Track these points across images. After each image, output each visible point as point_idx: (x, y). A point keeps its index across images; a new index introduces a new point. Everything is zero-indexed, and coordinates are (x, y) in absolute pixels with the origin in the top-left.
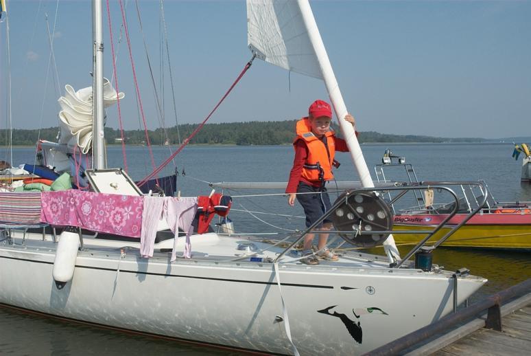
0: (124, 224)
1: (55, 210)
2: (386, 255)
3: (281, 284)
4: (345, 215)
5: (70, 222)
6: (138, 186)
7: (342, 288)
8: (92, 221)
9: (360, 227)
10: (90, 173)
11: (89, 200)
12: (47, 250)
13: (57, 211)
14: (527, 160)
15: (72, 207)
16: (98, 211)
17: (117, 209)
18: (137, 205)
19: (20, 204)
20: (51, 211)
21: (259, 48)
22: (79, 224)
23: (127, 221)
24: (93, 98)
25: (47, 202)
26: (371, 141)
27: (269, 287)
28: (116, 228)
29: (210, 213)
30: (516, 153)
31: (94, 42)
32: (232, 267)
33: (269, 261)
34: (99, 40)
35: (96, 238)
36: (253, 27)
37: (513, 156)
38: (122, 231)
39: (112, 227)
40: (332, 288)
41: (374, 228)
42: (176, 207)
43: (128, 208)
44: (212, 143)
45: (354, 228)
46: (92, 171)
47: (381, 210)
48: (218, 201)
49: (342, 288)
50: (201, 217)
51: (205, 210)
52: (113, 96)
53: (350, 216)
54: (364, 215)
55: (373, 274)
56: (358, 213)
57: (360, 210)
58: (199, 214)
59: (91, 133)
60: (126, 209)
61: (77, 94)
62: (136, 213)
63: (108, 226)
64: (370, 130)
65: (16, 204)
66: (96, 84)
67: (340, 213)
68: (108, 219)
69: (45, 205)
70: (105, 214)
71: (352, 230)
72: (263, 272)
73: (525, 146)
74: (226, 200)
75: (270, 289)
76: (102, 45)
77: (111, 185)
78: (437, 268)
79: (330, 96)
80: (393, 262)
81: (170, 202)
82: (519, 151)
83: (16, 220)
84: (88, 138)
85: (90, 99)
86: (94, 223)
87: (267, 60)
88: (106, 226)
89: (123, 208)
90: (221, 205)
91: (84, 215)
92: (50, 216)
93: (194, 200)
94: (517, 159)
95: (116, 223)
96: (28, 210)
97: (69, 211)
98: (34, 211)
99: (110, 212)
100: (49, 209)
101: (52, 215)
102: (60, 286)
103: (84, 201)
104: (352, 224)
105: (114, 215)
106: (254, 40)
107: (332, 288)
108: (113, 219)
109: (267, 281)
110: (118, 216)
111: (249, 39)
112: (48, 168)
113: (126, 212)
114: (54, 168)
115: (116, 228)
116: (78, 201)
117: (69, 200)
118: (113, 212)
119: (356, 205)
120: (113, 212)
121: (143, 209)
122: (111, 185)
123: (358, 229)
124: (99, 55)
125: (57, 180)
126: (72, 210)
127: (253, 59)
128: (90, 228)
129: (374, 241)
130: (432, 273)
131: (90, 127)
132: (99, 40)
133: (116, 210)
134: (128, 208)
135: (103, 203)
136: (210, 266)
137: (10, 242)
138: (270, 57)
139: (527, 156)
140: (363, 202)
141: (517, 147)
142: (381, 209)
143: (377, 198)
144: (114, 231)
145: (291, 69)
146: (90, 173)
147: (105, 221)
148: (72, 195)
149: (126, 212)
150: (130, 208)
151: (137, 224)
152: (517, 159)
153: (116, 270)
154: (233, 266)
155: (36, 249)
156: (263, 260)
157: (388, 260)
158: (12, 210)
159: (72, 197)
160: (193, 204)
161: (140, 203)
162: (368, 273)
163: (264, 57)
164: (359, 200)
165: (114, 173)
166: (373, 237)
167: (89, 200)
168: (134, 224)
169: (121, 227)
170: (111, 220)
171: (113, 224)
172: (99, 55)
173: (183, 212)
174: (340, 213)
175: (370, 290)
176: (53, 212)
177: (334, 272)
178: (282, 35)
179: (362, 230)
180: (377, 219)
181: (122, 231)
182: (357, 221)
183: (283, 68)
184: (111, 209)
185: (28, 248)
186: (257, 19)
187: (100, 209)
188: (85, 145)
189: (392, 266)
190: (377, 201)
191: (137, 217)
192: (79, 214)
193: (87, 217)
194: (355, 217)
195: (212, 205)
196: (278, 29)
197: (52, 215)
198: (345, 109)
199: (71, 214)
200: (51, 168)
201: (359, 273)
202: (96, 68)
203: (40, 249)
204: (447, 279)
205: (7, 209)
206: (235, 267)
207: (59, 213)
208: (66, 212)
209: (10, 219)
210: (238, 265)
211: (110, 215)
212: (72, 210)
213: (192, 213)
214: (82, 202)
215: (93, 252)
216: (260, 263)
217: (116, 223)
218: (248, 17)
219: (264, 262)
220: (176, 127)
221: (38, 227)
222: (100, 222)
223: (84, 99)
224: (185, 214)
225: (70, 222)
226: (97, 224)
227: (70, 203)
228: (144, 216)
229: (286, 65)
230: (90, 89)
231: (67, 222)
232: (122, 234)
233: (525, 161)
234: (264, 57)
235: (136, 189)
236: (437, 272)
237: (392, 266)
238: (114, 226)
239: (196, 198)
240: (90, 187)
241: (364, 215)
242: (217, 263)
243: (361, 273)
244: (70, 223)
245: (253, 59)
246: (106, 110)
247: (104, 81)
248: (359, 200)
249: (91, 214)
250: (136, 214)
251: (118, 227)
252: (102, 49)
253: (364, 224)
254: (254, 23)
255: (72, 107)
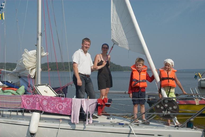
0: (63, 109)
1: (28, 103)
2: (173, 122)
3: (136, 134)
4: (160, 107)
5: (36, 108)
6: (55, 91)
7: (158, 135)
8: (48, 108)
9: (166, 112)
10: (36, 86)
11: (46, 99)
12: (24, 120)
13: (29, 103)
14: (200, 79)
15: (37, 102)
16: (51, 104)
17: (60, 103)
18: (69, 102)
19: (15, 100)
20: (26, 104)
21: (116, 40)
22: (41, 109)
23: (32, 103)
24: (37, 55)
25: (24, 100)
26: (127, 70)
27: (130, 135)
28: (60, 111)
29: (103, 106)
30: (196, 77)
31: (38, 32)
32: (111, 127)
33: (127, 125)
34: (40, 31)
35: (43, 114)
36: (113, 32)
37: (195, 78)
38: (62, 112)
39: (58, 111)
40: (154, 135)
41: (171, 112)
42: (87, 103)
43: (65, 103)
44: (61, 71)
45: (163, 112)
46: (36, 85)
47: (175, 105)
48: (107, 101)
49: (158, 135)
50: (99, 107)
51: (101, 104)
52: (44, 54)
53: (162, 108)
54: (168, 107)
55: (148, 129)
56: (165, 106)
57: (166, 105)
58: (97, 106)
59: (35, 69)
60: (64, 103)
61: (29, 52)
62: (34, 100)
63: (55, 110)
64: (127, 66)
65: (8, 100)
66: (38, 49)
67: (158, 107)
68: (56, 107)
69: (24, 101)
70: (54, 105)
71: (163, 113)
72: (126, 129)
73: (199, 74)
74: (110, 101)
75: (130, 136)
76: (41, 33)
77: (45, 91)
78: (195, 127)
79: (148, 61)
80: (176, 125)
81: (84, 101)
82: (197, 75)
83: (8, 107)
84: (34, 71)
85: (35, 55)
86: (49, 109)
87: (119, 45)
88: (55, 110)
89: (30, 98)
90: (108, 103)
91: (43, 106)
92: (26, 105)
93: (95, 100)
94: (196, 79)
95: (60, 109)
96: (15, 103)
97: (35, 104)
98: (18, 103)
99: (56, 104)
100: (25, 103)
101: (27, 105)
102: (32, 135)
103: (43, 100)
104: (163, 111)
105: (59, 106)
106: (114, 37)
107: (154, 135)
108: (58, 107)
109: (128, 133)
110: (61, 106)
111: (112, 37)
112: (9, 82)
113: (64, 104)
114: (12, 82)
115: (60, 111)
116: (40, 101)
117: (36, 99)
118: (58, 105)
119: (165, 103)
120: (58, 105)
121: (72, 103)
122: (45, 91)
123: (165, 113)
124: (40, 37)
125: (19, 89)
126: (37, 103)
127: (114, 45)
128: (47, 111)
129: (171, 117)
130: (194, 129)
131: (35, 67)
132: (40, 31)
133: (27, 99)
134: (65, 103)
135: (53, 101)
136: (101, 126)
137: (3, 116)
138: (120, 44)
139: (200, 78)
140: (168, 102)
141: (196, 74)
142: (175, 105)
143: (174, 101)
144: (59, 112)
145: (130, 49)
146: (36, 86)
147: (54, 108)
148: (38, 97)
149: (64, 104)
150: (66, 103)
151: (69, 109)
152: (196, 79)
153: (59, 128)
154: (102, 126)
155: (17, 119)
156: (124, 124)
157: (174, 124)
158: (6, 103)
159: (38, 97)
160: (95, 102)
161: (71, 101)
162: (169, 130)
163: (118, 44)
164: (166, 101)
165: (45, 86)
166: (171, 116)
167: (46, 99)
168: (68, 109)
169: (62, 111)
170: (57, 107)
171: (58, 109)
172: (40, 37)
173: (90, 105)
174: (158, 107)
175: (170, 136)
176: (27, 104)
177: (155, 129)
178: (126, 36)
179: (167, 113)
180: (173, 109)
181: (62, 112)
182: (165, 109)
183: (126, 49)
184: (57, 104)
185: (13, 119)
186: (115, 29)
187: (52, 103)
188: (32, 74)
189: (176, 126)
190: (174, 102)
191: (69, 107)
192: (40, 105)
193: (45, 106)
194: (164, 108)
195: (104, 102)
196: (124, 34)
197: (27, 105)
198: (154, 66)
199: (36, 105)
200: (10, 82)
201: (154, 129)
202: (38, 42)
203: (19, 119)
204: (201, 132)
205: (3, 102)
206: (103, 127)
207: (30, 104)
208: (34, 104)
209: (5, 107)
210: (113, 126)
211: (57, 106)
212: (37, 103)
213: (95, 105)
214: (42, 100)
215: (46, 121)
216: (123, 125)
217: (60, 109)
218: (111, 29)
219: (125, 125)
220: (48, 63)
221: (20, 110)
222: (52, 109)
223: (32, 55)
224: (90, 106)
225: (36, 108)
226: (50, 109)
227: (36, 100)
228: (73, 106)
229: (127, 48)
230: (35, 51)
231: (35, 108)
232: (62, 113)
233: (199, 80)
234: (118, 44)
235: (54, 92)
236: (195, 129)
237: (176, 126)
238: (59, 110)
239: (96, 100)
240: (35, 92)
241: (168, 107)
242: (104, 125)
243: (144, 128)
244: (36, 109)
245: (114, 45)
246: (42, 58)
247: (42, 48)
248: (166, 101)
249: (48, 105)
250: (69, 105)
251: (61, 111)
252: (41, 35)
253: (168, 111)
254: (114, 31)
255: (28, 58)
